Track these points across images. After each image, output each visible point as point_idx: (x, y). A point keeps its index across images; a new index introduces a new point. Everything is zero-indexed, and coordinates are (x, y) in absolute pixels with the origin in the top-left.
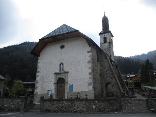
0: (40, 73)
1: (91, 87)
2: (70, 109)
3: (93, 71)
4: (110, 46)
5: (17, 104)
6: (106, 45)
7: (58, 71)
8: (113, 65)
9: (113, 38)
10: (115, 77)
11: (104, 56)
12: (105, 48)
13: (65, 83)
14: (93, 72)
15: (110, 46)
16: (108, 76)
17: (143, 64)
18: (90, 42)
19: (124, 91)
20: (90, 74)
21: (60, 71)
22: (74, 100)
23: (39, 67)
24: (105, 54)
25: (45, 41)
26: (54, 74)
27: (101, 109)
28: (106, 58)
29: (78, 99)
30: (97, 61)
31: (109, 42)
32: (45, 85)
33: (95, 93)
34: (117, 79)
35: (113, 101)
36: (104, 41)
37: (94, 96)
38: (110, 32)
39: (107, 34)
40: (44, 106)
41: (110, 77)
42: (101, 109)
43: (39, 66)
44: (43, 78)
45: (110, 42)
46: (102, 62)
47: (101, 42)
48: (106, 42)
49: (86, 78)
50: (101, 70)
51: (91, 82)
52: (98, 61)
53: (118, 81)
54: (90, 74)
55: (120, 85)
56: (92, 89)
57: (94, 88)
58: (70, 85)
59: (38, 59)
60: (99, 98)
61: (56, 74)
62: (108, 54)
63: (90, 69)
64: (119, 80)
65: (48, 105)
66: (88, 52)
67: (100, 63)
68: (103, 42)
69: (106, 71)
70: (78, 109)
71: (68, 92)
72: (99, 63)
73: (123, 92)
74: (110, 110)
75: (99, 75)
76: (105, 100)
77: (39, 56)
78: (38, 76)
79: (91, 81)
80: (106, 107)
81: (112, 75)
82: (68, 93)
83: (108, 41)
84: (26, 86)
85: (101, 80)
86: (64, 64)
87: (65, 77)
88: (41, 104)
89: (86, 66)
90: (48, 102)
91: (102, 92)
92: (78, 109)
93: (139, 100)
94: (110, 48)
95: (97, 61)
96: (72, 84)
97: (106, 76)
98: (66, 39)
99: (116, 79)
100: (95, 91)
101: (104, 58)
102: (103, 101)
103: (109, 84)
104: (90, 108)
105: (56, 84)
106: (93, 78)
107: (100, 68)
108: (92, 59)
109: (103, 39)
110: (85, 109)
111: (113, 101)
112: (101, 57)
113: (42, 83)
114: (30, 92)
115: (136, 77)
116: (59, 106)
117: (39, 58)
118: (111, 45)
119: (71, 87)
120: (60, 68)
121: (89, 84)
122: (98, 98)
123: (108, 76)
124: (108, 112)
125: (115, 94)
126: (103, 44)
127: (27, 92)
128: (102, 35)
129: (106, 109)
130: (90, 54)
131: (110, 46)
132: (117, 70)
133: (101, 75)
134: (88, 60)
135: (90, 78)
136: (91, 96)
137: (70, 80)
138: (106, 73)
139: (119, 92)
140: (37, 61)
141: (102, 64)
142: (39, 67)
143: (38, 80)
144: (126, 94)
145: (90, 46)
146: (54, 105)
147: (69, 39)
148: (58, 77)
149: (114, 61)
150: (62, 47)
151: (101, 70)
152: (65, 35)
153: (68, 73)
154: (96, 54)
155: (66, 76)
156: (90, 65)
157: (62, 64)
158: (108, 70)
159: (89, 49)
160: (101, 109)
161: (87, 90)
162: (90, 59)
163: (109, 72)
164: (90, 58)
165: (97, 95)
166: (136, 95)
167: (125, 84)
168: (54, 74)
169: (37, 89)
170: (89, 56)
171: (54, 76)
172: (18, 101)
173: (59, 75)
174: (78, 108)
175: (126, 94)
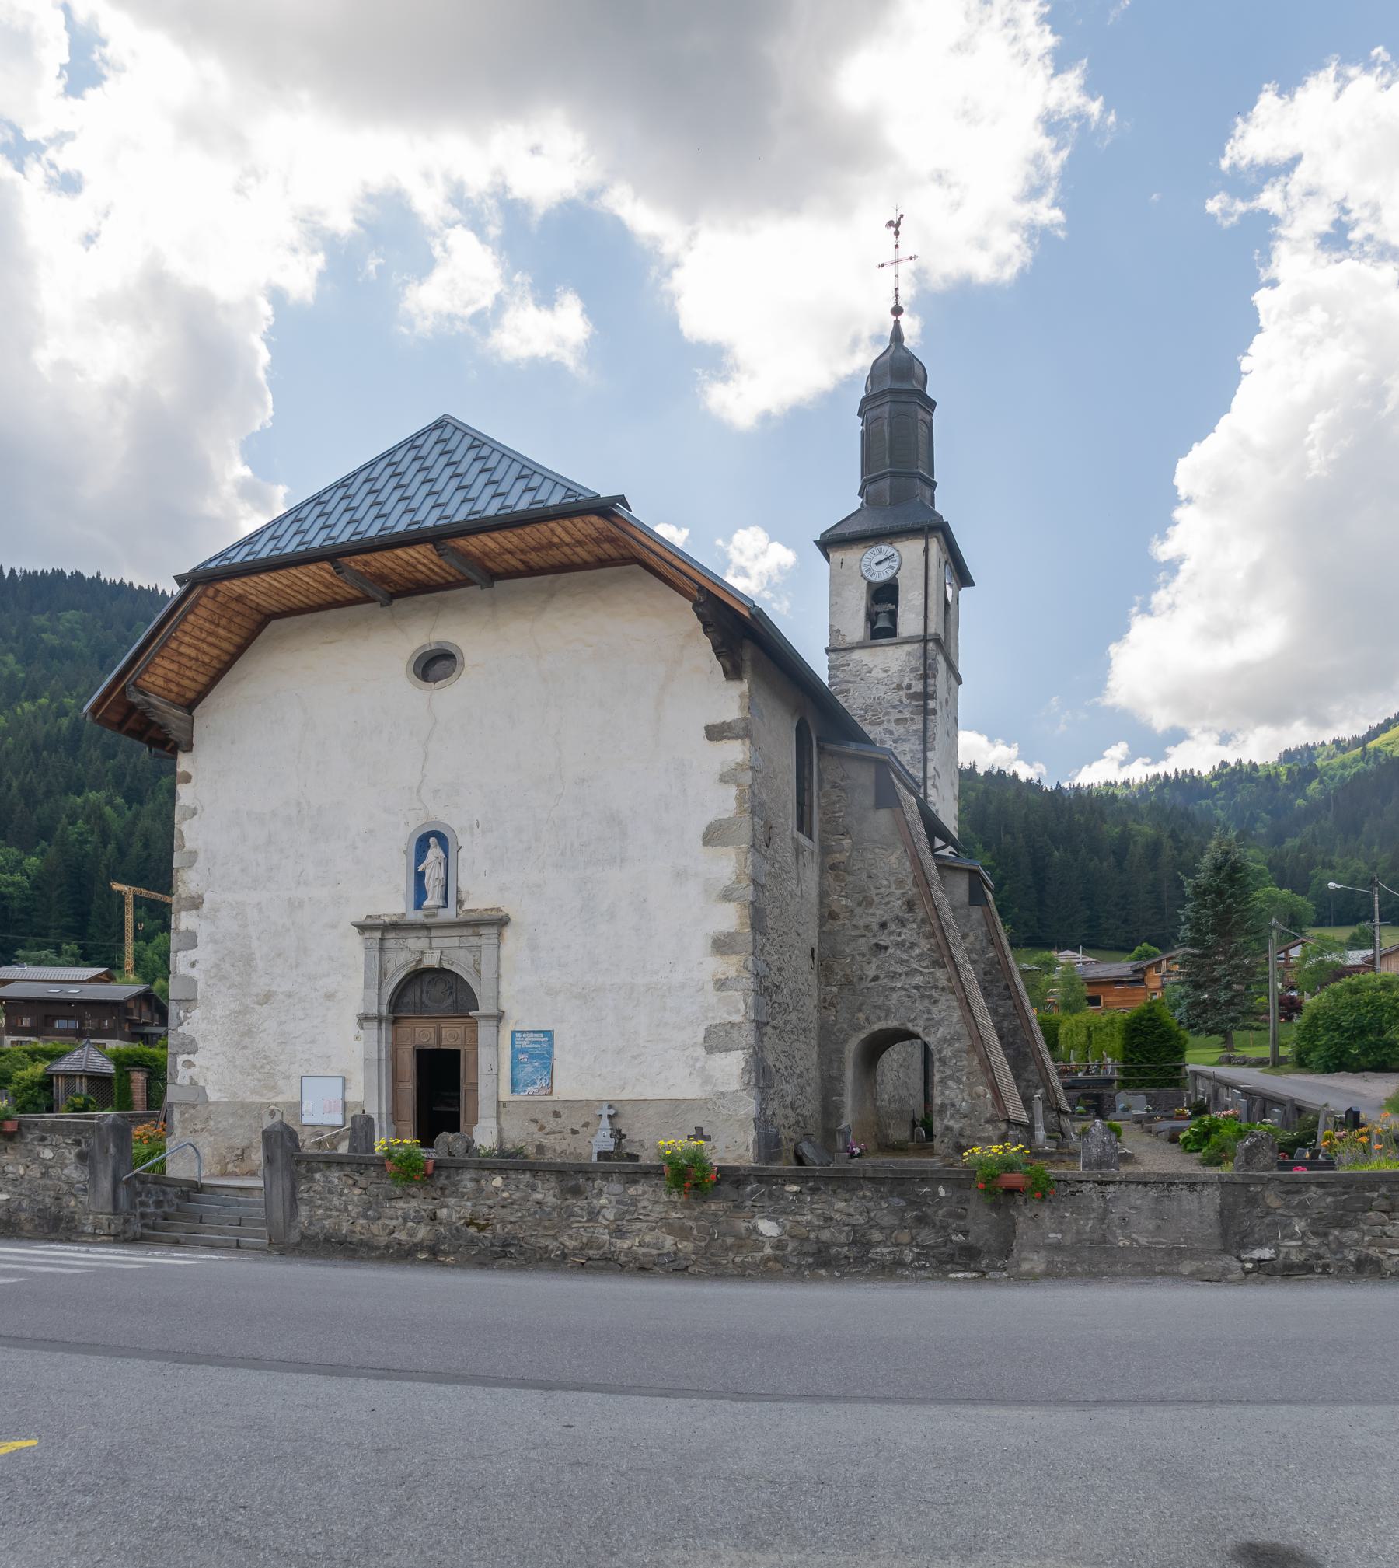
0: (215, 910)
1: (730, 1069)
2: (543, 1242)
3: (757, 919)
4: (927, 673)
5: (44, 1175)
6: (890, 662)
7: (395, 904)
8: (943, 866)
9: (965, 592)
10: (958, 988)
11: (864, 776)
12: (879, 691)
13: (475, 1022)
14: (754, 927)
15: (925, 677)
16: (894, 976)
17: (585, 341)
18: (740, 635)
19: (1027, 1103)
20: (722, 945)
21: (418, 906)
22: (584, 1171)
23: (193, 856)
24: (884, 766)
25: (240, 599)
26: (362, 928)
27: (834, 1251)
28: (886, 799)
29: (622, 1163)
30: (792, 822)
31: (924, 640)
32: (273, 1031)
33: (762, 1122)
34: (979, 1004)
35: (942, 1192)
36: (871, 618)
37: (757, 1142)
38: (942, 530)
39: (910, 550)
40: (304, 1210)
41: (918, 979)
42: (834, 1251)
43: (189, 845)
44: (248, 960)
45: (937, 640)
46: (847, 843)
47: (834, 632)
48: (891, 632)
49: (683, 986)
50: (833, 916)
51: (737, 1018)
52: (803, 824)
53: (986, 1021)
54: (722, 945)
55: (998, 1058)
56: (735, 1085)
57: (762, 1076)
58: (524, 1042)
59: (173, 770)
60: (800, 1160)
61: (380, 930)
62: (906, 753)
63: (726, 896)
64: (993, 1011)
65: (338, 1203)
66: (716, 733)
67: (825, 850)
68: (856, 628)
69: (874, 923)
70: (625, 1244)
71: (505, 1094)
72: (816, 848)
73: (1023, 1117)
74: (908, 1256)
75: (805, 964)
76: (871, 1179)
77: (189, 747)
78: (191, 940)
79: (736, 1009)
80: (877, 1236)
81: (936, 964)
82: (500, 1105)
83: (909, 622)
84: (26, 1022)
85: (825, 1004)
86: (463, 840)
87: (477, 962)
88: (267, 1191)
89: (680, 875)
90: (335, 1177)
91: (830, 1110)
92: (625, 1244)
93: (1167, 1183)
94: (926, 695)
95: (800, 829)
96: (549, 1034)
97: (871, 971)
98: (367, 599)
99: (966, 1005)
100: (763, 1100)
101: (869, 800)
102: (844, 1182)
103: (897, 1047)
104: (730, 1241)
105: (380, 1019)
106: (748, 981)
107: (823, 895)
108: (755, 807)
109: (857, 601)
110: (687, 1246)
111: (942, 1192)
112: (834, 786)
113: (244, 1011)
114: (97, 1080)
115: (1138, 979)
116: (443, 1213)
117: (184, 763)
118: (942, 665)
119: (539, 1053)
120: (420, 877)
121: (715, 1041)
122: (800, 1155)
123: (894, 976)
124: (891, 1270)
125: (948, 1129)
126: (857, 655)
127: (69, 1077)
128: (851, 556)
129: (871, 1245)
130: (735, 751)
131: (927, 673)
132: (976, 913)
133: (825, 962)
134: (710, 818)
135: (721, 984)
136: (734, 1145)
137: (522, 988)
138: (879, 948)
139: (989, 1112)
140: (172, 794)
141: (839, 857)
142: (193, 856)
143: (193, 982)
144: (1041, 1134)
145: (733, 672)
146: (401, 1204)
147: (499, 585)
148: (402, 957)
149: (951, 824)
150: (434, 665)
151: (828, 916)
152: (472, 544)
153: (508, 932)
154: (787, 760)
155: (488, 953)
156: (726, 865)
157: (431, 840)
158: (902, 923)
159: (728, 700)
160: (827, 1246)
161: (688, 1089)
162: (732, 805)
163: (908, 934)
164: (733, 791)
165: (784, 1134)
166: (1133, 1141)
167: (1036, 1027)
168: (362, 928)
169: (195, 1059)
170: (723, 779)
171: (355, 948)
172: (47, 1154)
173: (412, 943)
174: (619, 1233)
175: (1041, 1134)
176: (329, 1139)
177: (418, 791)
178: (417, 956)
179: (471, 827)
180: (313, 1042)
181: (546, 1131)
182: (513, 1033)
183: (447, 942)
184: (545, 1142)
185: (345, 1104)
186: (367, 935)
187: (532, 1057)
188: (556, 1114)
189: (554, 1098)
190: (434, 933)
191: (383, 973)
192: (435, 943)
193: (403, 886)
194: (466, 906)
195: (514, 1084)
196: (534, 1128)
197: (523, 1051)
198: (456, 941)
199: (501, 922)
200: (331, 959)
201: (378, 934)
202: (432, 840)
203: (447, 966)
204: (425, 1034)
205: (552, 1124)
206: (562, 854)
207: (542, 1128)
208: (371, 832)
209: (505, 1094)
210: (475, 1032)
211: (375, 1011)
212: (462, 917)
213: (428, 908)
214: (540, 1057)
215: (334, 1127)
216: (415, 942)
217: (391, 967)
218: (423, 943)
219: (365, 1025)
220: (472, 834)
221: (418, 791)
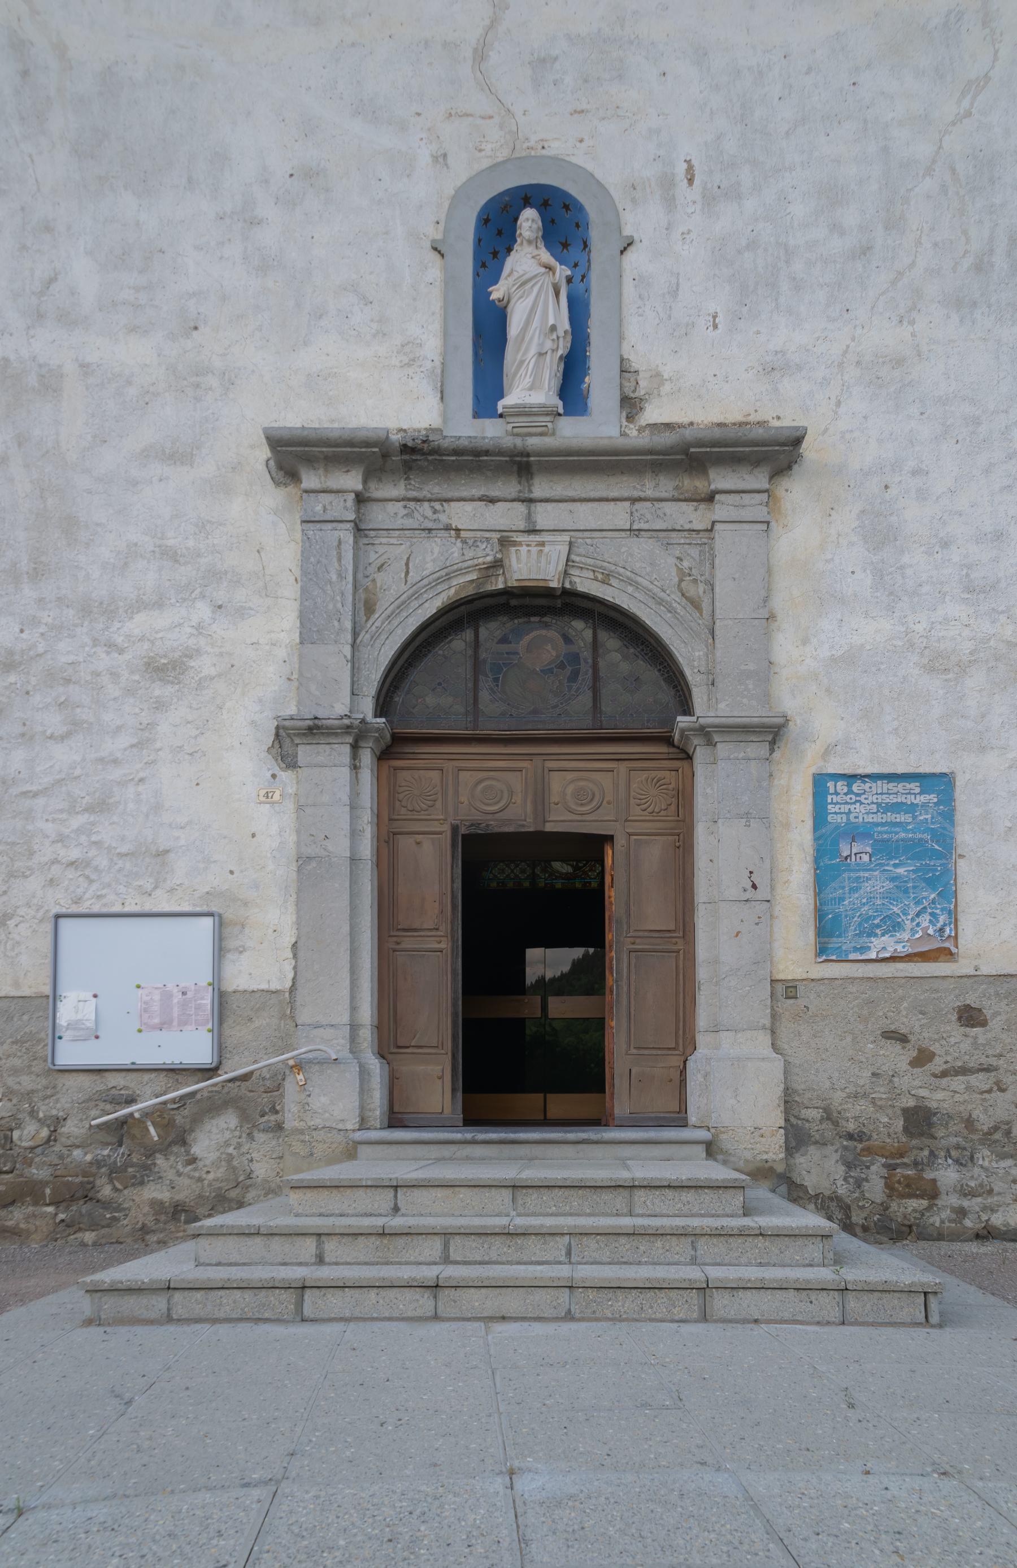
7: (407, 398)
26: (294, 456)
58: (861, 808)
86: (640, 220)
96: (939, 783)
105: (357, 735)
153: (795, 492)
171: (264, 529)
173: (463, 514)
176: (160, 1115)
177: (480, 55)
178: (486, 554)
179: (667, 183)
180: (101, 806)
181: (938, 1065)
182: (820, 782)
183: (586, 516)
184: (940, 1098)
185: (222, 1000)
186: (310, 480)
187: (886, 849)
188: (970, 1017)
189: (963, 967)
190: (541, 487)
191: (366, 605)
192: (546, 516)
193: (431, 346)
194: (653, 414)
195: (826, 931)
196: (896, 1058)
197: (855, 833)
198: (618, 515)
199: (775, 454)
200: (171, 556)
201: (352, 480)
202: (529, 221)
203: (585, 584)
204: (498, 792)
205: (956, 1043)
206: (980, 267)
207: (922, 1058)
208: (309, 175)
209: (794, 954)
210: (683, 801)
211: (341, 707)
212: (635, 437)
213: (523, 411)
214: (913, 849)
215: (175, 1072)
216: (478, 514)
217: (391, 586)
218: (506, 516)
219: (304, 753)
220: (670, 202)
221: (480, 55)
